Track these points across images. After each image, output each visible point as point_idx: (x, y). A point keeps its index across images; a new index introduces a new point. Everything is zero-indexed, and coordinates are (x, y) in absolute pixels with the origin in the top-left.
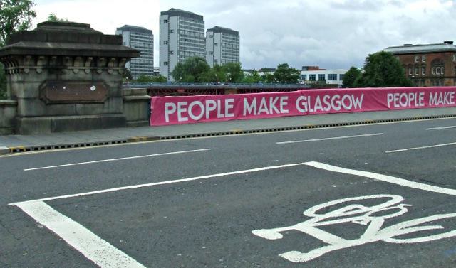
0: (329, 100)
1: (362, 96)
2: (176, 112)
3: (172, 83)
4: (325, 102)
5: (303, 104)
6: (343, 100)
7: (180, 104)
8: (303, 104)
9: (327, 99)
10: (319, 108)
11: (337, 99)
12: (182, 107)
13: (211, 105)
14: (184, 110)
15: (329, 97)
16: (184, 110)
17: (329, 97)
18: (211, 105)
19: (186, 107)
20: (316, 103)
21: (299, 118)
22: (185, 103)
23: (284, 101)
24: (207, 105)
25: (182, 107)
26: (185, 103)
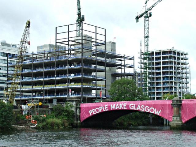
0: (144, 108)
1: (160, 111)
2: (92, 112)
3: (93, 68)
4: (142, 107)
5: (147, 109)
6: (150, 109)
7: (93, 110)
8: (147, 109)
9: (143, 107)
10: (118, 108)
11: (147, 108)
12: (94, 110)
13: (101, 108)
14: (94, 111)
15: (144, 106)
16: (94, 111)
17: (144, 106)
18: (101, 108)
19: (95, 110)
20: (138, 107)
21: (148, 104)
22: (94, 109)
23: (106, 107)
24: (100, 108)
25: (94, 110)
26: (94, 109)
